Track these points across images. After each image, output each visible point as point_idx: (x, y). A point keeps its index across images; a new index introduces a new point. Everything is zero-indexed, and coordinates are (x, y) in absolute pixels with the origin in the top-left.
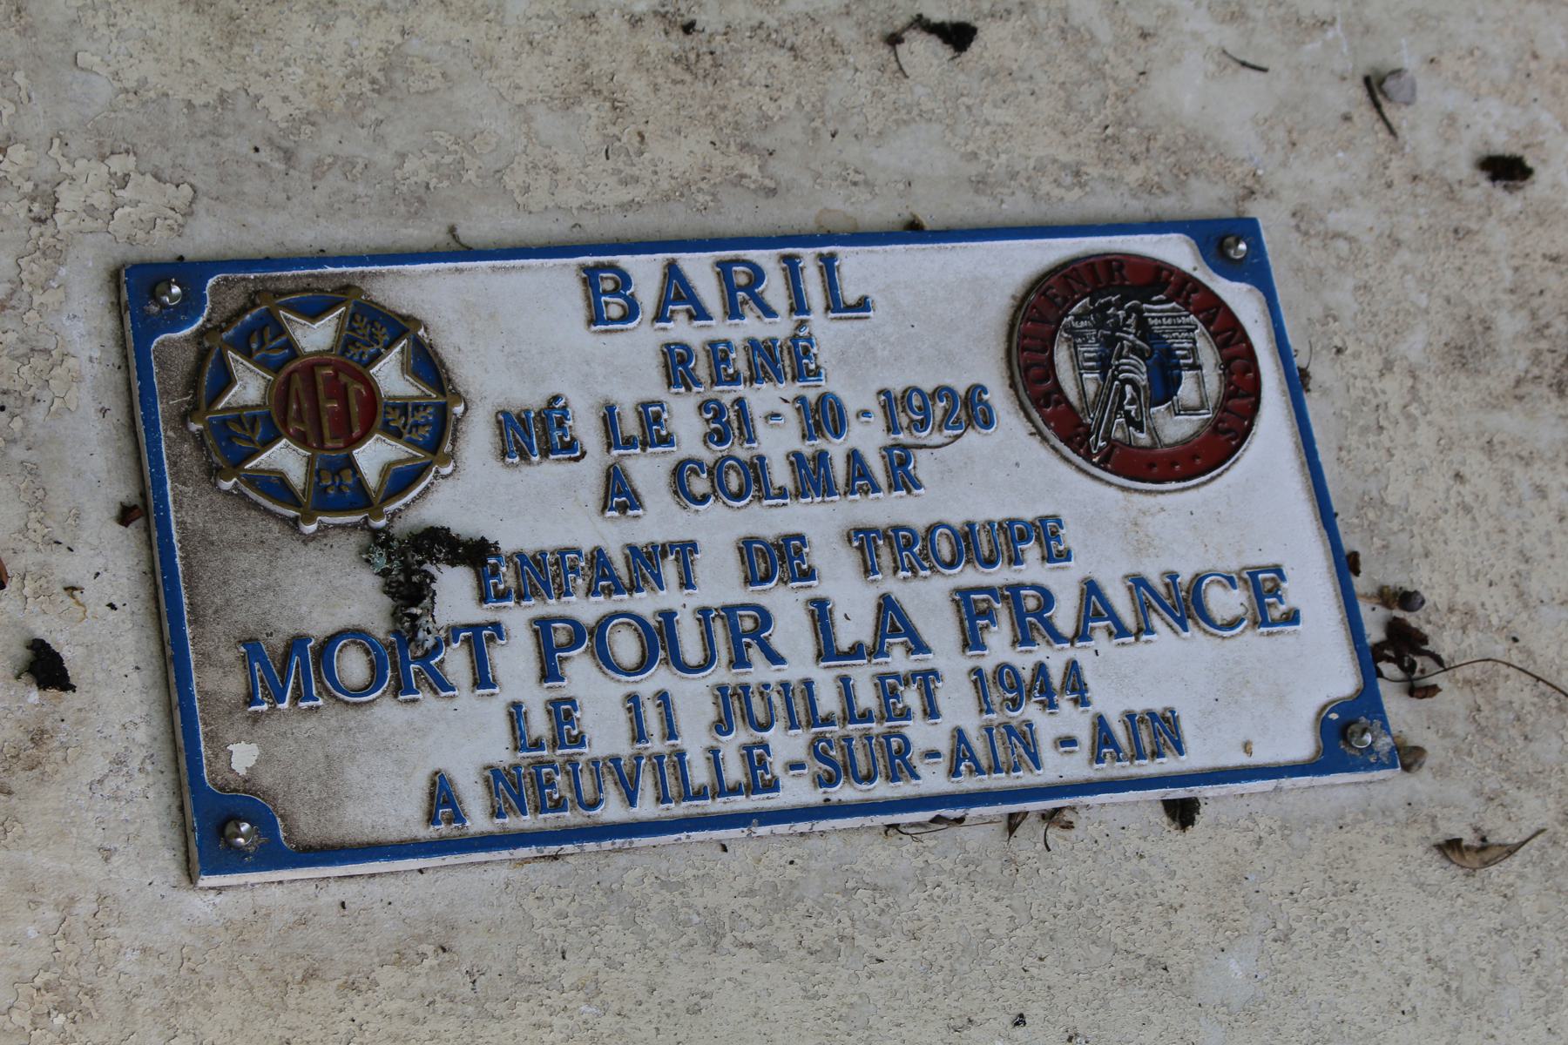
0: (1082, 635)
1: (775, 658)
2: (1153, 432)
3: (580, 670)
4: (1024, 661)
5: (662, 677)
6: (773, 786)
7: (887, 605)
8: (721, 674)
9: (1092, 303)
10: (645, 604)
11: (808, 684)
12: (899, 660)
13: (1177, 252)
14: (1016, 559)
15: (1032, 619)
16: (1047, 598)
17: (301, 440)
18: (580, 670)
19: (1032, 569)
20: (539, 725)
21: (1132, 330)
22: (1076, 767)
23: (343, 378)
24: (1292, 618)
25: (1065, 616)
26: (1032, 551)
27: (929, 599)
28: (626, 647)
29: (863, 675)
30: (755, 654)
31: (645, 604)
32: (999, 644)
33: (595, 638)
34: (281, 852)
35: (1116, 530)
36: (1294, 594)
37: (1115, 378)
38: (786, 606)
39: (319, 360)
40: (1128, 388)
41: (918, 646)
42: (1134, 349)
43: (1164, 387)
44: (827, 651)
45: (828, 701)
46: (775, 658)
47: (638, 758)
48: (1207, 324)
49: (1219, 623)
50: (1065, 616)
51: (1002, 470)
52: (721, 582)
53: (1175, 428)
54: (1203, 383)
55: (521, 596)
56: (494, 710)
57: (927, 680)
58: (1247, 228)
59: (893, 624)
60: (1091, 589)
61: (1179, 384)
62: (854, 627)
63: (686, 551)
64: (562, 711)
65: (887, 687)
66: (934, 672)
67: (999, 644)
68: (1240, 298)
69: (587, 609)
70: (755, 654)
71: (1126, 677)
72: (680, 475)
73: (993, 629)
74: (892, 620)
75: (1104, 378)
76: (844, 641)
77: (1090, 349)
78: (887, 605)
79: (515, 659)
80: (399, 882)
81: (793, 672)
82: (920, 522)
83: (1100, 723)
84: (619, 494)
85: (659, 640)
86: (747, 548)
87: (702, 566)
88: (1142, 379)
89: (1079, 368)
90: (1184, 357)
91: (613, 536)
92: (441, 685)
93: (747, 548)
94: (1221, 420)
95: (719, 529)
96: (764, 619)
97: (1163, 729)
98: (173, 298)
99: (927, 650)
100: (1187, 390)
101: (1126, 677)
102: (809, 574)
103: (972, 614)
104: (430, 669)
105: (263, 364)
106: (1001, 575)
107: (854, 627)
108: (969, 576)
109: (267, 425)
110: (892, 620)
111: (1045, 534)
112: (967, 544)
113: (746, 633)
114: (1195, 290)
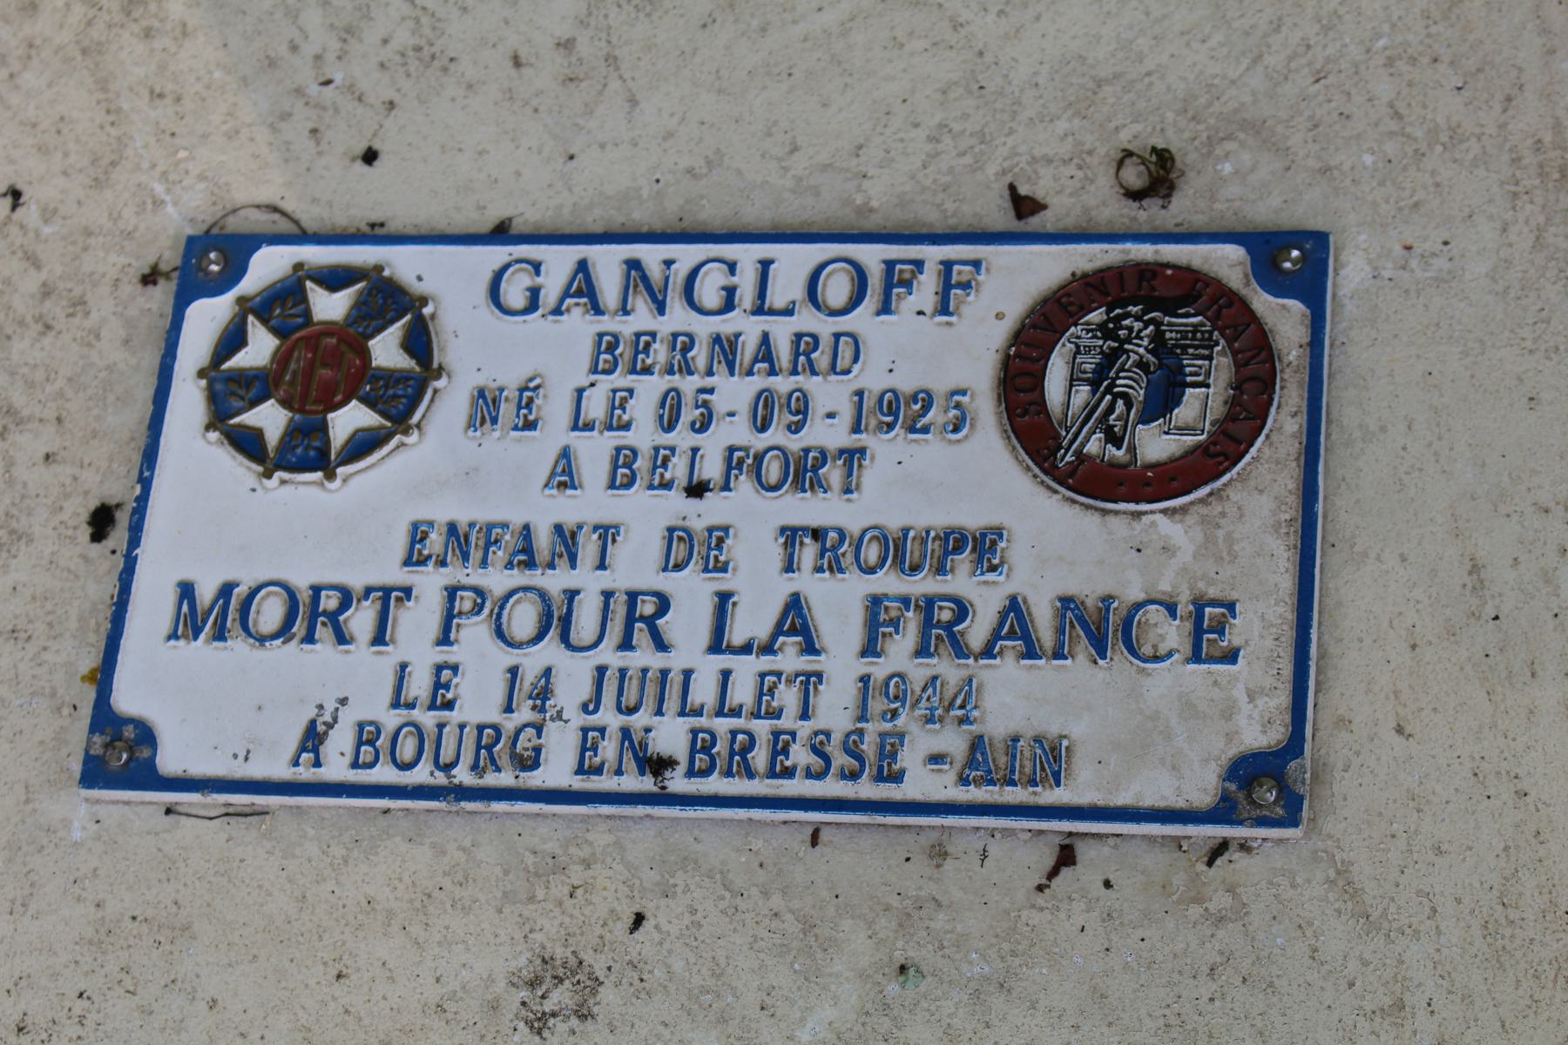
0: (988, 652)
1: (661, 645)
2: (1132, 449)
3: (474, 634)
4: (918, 672)
5: (549, 652)
6: (897, 777)
7: (795, 604)
8: (607, 655)
9: (1108, 313)
10: (555, 581)
11: (687, 674)
12: (790, 659)
13: (1226, 262)
14: (940, 569)
15: (942, 627)
16: (962, 610)
17: (285, 403)
18: (474, 634)
19: (961, 581)
20: (419, 685)
21: (1145, 342)
22: (942, 786)
23: (343, 347)
24: (1231, 656)
25: (977, 631)
26: (964, 559)
27: (838, 603)
28: (523, 618)
29: (746, 670)
30: (641, 634)
31: (555, 581)
32: (899, 651)
33: (498, 613)
34: (144, 776)
35: (1060, 546)
36: (1242, 629)
37: (1109, 390)
38: (692, 595)
39: (329, 328)
40: (1120, 402)
41: (810, 648)
42: (1142, 365)
43: (1161, 403)
44: (717, 645)
45: (704, 691)
46: (661, 645)
47: (441, 726)
48: (1230, 342)
49: (252, 630)
50: (977, 631)
51: (982, 477)
52: (636, 565)
53: (1156, 445)
54: (1202, 405)
55: (442, 563)
56: (383, 665)
57: (810, 681)
58: (1316, 245)
59: (1012, 625)
60: (1014, 607)
61: (1178, 403)
62: (751, 622)
63: (607, 533)
64: (444, 676)
65: (766, 685)
66: (819, 675)
67: (899, 651)
68: (1283, 317)
69: (497, 580)
70: (641, 634)
71: (1014, 696)
72: (623, 459)
73: (896, 637)
74: (795, 620)
75: (1094, 392)
76: (737, 636)
77: (1089, 363)
78: (795, 604)
79: (417, 624)
80: (1106, 850)
81: (676, 661)
82: (854, 527)
83: (977, 743)
84: (565, 475)
85: (556, 620)
86: (791, 536)
87: (620, 554)
88: (1139, 395)
89: (1073, 381)
90: (1192, 374)
91: (547, 512)
92: (342, 638)
93: (791, 536)
94: (1215, 443)
95: (647, 515)
96: (664, 604)
97: (1052, 758)
98: (1294, 262)
99: (816, 652)
100: (1187, 411)
101: (1014, 696)
102: (723, 568)
103: (878, 622)
104: (952, 636)
105: (276, 331)
106: (923, 585)
107: (751, 622)
108: (889, 582)
109: (256, 386)
110: (795, 620)
111: (983, 547)
112: (897, 549)
113: (642, 617)
114: (1230, 305)
